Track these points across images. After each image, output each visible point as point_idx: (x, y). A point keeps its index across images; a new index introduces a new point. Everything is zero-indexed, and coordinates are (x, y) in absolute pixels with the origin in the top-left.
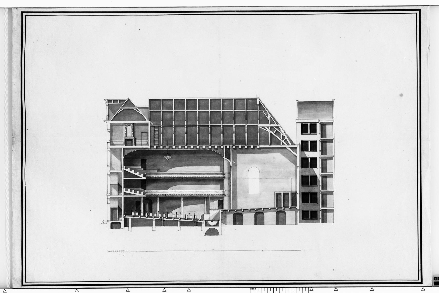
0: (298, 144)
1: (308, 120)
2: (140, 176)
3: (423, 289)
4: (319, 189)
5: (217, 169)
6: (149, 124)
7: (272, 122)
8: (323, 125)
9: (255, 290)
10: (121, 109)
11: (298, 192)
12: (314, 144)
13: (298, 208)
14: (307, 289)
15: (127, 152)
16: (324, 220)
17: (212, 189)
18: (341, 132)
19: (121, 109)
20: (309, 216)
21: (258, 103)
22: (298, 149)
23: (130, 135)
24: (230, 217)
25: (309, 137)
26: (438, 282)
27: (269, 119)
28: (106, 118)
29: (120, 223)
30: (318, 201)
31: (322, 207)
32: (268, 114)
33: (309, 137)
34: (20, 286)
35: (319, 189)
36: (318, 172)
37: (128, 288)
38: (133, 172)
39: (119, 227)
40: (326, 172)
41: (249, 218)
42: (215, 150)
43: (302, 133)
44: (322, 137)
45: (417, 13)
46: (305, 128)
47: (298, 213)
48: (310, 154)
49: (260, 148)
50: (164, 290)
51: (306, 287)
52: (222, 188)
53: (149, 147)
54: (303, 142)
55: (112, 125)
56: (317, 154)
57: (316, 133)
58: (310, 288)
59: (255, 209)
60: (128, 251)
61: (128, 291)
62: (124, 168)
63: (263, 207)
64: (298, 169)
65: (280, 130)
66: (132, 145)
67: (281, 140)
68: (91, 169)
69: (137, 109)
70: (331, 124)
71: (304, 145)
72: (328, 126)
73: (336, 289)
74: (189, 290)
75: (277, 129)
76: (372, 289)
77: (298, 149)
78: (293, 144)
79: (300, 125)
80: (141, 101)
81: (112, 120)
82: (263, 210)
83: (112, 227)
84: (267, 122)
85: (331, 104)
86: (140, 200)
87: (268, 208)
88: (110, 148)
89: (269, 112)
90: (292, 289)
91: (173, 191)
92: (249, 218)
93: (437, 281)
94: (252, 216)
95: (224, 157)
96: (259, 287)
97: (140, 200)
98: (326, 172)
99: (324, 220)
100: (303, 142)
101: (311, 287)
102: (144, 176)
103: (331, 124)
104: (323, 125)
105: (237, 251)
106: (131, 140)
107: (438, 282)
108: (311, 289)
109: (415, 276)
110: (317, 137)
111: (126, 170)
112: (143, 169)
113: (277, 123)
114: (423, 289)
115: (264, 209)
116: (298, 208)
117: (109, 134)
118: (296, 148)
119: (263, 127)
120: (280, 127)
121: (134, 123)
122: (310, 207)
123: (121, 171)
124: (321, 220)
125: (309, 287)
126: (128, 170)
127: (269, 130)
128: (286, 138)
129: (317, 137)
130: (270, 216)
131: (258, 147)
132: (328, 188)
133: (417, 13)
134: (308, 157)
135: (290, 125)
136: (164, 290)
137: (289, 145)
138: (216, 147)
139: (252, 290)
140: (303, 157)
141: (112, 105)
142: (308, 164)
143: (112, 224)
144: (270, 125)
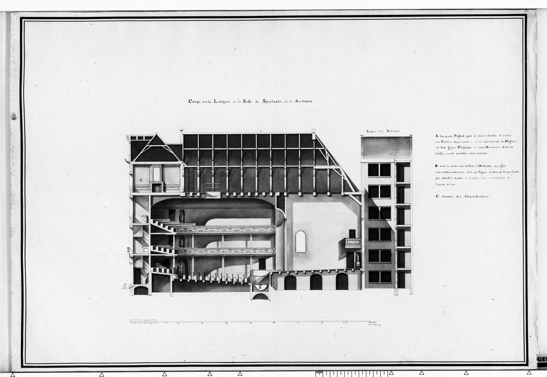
0: (364, 190)
2: (169, 231)
3: (529, 373)
5: (267, 222)
7: (331, 163)
8: (401, 167)
9: (321, 374)
10: (147, 147)
12: (386, 191)
14: (386, 372)
15: (156, 201)
16: (401, 284)
17: (261, 246)
20: (378, 278)
21: (314, 138)
23: (157, 179)
24: (281, 281)
25: (379, 181)
26: (545, 363)
28: (129, 159)
29: (147, 289)
30: (368, 255)
32: (327, 152)
33: (379, 181)
34: (19, 369)
35: (393, 245)
36: (392, 223)
38: (161, 226)
39: (147, 293)
40: (404, 203)
41: (303, 282)
42: (256, 197)
43: (369, 175)
44: (398, 202)
46: (373, 170)
47: (363, 275)
48: (380, 202)
49: (345, 196)
52: (274, 245)
54: (370, 187)
55: (134, 166)
56: (391, 202)
58: (389, 372)
59: (311, 271)
61: (165, 375)
62: (151, 221)
63: (320, 268)
64: (363, 222)
66: (160, 192)
68: (95, 216)
70: (408, 165)
71: (373, 191)
72: (406, 169)
73: (422, 373)
74: (240, 374)
78: (356, 190)
79: (367, 164)
81: (136, 161)
82: (322, 273)
83: (135, 293)
85: (408, 139)
86: (172, 260)
87: (327, 270)
88: (134, 196)
91: (212, 248)
92: (303, 282)
93: (542, 362)
94: (307, 279)
95: (276, 207)
97: (172, 260)
99: (401, 284)
100: (370, 187)
101: (391, 371)
102: (175, 230)
103: (408, 165)
104: (401, 167)
106: (159, 185)
107: (545, 363)
108: (391, 373)
110: (391, 181)
111: (154, 224)
112: (169, 220)
113: (338, 164)
115: (322, 271)
117: (132, 178)
118: (360, 196)
120: (341, 170)
121: (163, 165)
122: (379, 267)
123: (147, 224)
124: (396, 285)
126: (156, 224)
130: (329, 281)
132: (406, 245)
134: (377, 205)
135: (354, 168)
136: (210, 374)
138: (264, 194)
139: (317, 374)
140: (371, 205)
142: (375, 213)
143: (136, 289)
144: (328, 167)
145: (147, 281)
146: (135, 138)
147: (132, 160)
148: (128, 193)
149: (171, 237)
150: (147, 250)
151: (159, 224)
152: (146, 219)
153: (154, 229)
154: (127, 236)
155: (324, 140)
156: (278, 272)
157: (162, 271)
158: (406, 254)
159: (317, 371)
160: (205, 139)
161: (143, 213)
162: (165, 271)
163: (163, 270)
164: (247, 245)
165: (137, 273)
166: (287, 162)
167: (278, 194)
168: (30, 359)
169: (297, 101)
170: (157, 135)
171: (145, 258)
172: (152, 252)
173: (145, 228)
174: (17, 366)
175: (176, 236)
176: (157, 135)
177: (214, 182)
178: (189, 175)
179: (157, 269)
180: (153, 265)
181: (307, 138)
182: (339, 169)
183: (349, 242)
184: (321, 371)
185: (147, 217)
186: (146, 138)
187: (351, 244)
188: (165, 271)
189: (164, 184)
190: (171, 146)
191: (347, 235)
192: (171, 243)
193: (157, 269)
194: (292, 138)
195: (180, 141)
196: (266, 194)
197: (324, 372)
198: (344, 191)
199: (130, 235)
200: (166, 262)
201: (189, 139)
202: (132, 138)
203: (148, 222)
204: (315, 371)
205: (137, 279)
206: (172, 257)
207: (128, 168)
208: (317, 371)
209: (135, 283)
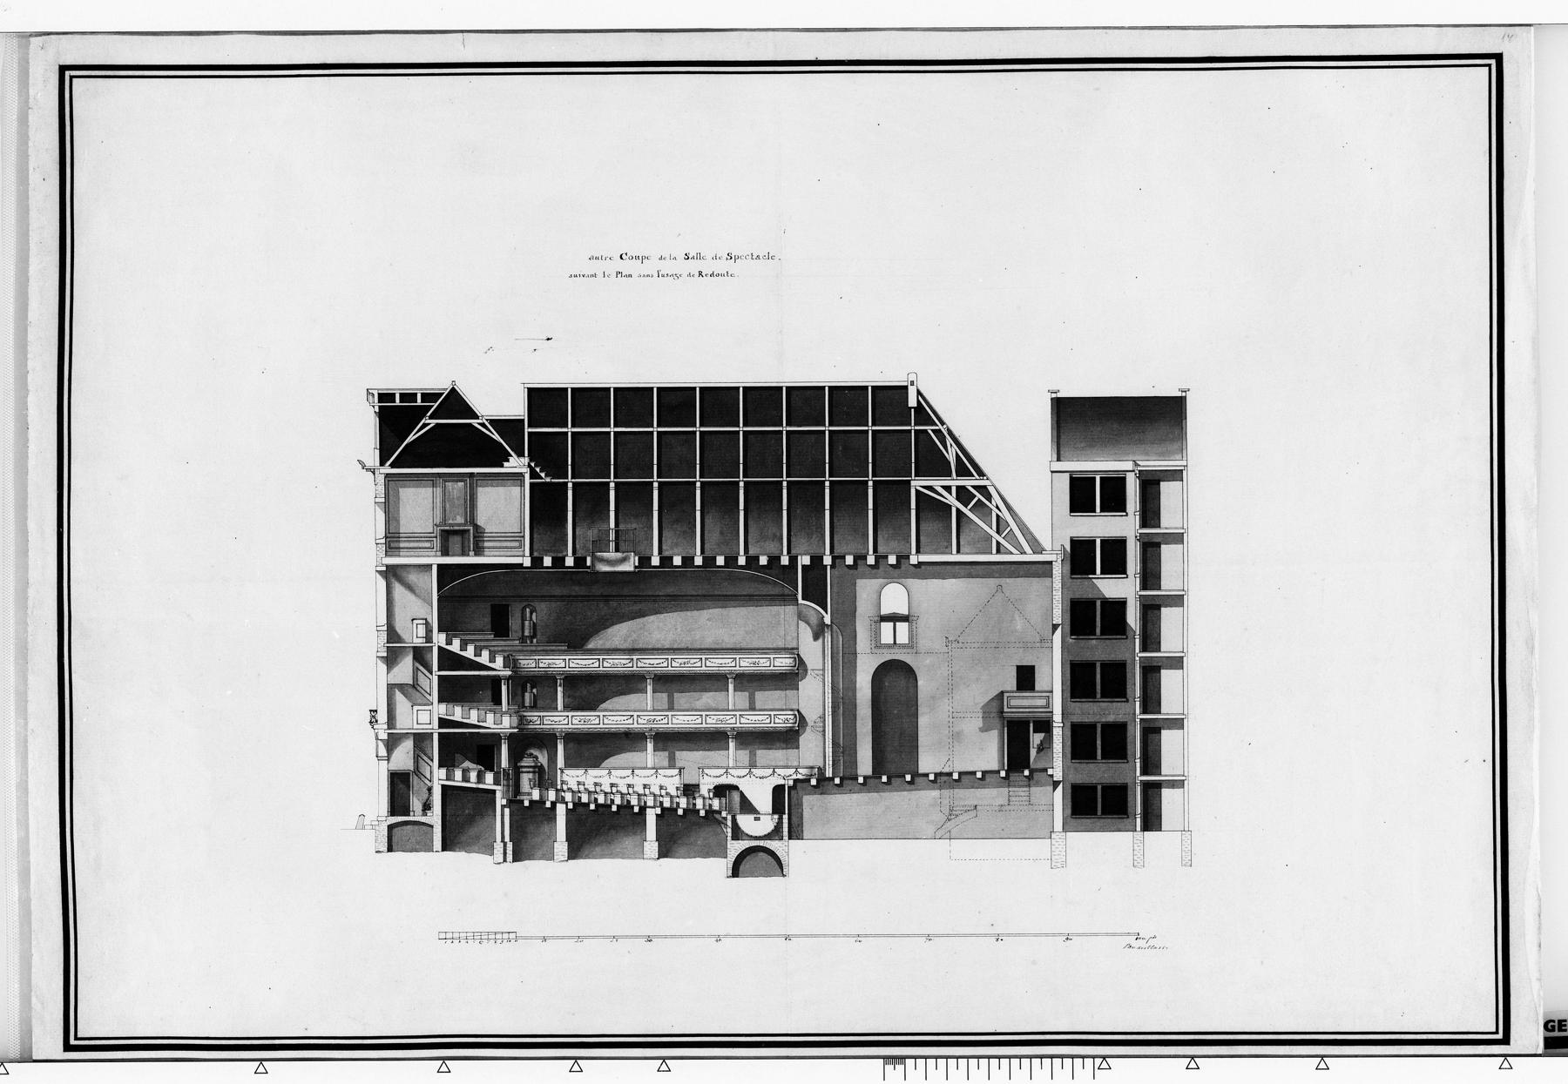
1: (1098, 464)
3: (1506, 1065)
4: (1132, 712)
6: (527, 476)
7: (963, 471)
9: (900, 1068)
10: (425, 425)
11: (1057, 718)
12: (1114, 554)
13: (1058, 776)
14: (1089, 1061)
16: (1152, 821)
18: (1215, 503)
19: (425, 425)
20: (1096, 805)
21: (912, 402)
22: (1057, 570)
25: (1099, 526)
26: (1565, 1038)
27: (952, 458)
28: (373, 458)
31: (1144, 711)
32: (949, 441)
33: (1099, 526)
34: (57, 1051)
35: (1132, 712)
37: (444, 1059)
38: (469, 653)
40: (1159, 588)
44: (1145, 585)
46: (1082, 495)
49: (920, 564)
51: (936, 1057)
53: (527, 562)
57: (1124, 509)
58: (1098, 1061)
60: (511, 936)
62: (440, 639)
65: (989, 497)
66: (464, 553)
67: (993, 533)
68: (278, 617)
69: (483, 425)
70: (1176, 475)
71: (1081, 555)
73: (1193, 1065)
74: (664, 1067)
75: (979, 496)
77: (1057, 570)
78: (1037, 548)
80: (497, 398)
81: (392, 466)
84: (942, 469)
89: (950, 432)
90: (1015, 1062)
91: (612, 717)
93: (1556, 1034)
96: (989, 1057)
98: (1159, 588)
99: (1152, 821)
101: (1104, 1057)
103: (1176, 475)
104: (1151, 484)
106: (463, 533)
108: (1104, 1065)
110: (1125, 526)
113: (981, 474)
114: (1506, 1065)
116: (1058, 776)
119: (930, 488)
120: (991, 489)
122: (1099, 772)
125: (1094, 1057)
126: (455, 647)
127: (951, 499)
129: (1125, 526)
131: (914, 560)
132: (1164, 522)
135: (1028, 481)
139: (889, 1068)
144: (955, 482)
145: (427, 807)
146: (391, 397)
147: (382, 463)
148: (371, 557)
149: (496, 682)
150: (426, 716)
151: (463, 648)
152: (422, 631)
153: (448, 659)
154: (369, 681)
155: (940, 403)
156: (950, 774)
157: (467, 776)
158: (1163, 732)
159: (886, 1058)
160: (590, 401)
161: (419, 613)
162: (480, 778)
163: (473, 776)
164: (522, 719)
165: (399, 785)
166: (832, 467)
167: (805, 560)
168: (91, 1025)
169: (700, 274)
170: (453, 390)
171: (421, 740)
172: (443, 723)
173: (420, 655)
174: (49, 1040)
175: (508, 679)
176: (453, 390)
177: (617, 524)
178: (546, 509)
179: (458, 774)
180: (447, 762)
181: (891, 399)
182: (985, 487)
183: (1014, 702)
184: (901, 1059)
185: (428, 625)
186: (425, 397)
187: (1023, 704)
188: (480, 778)
189: (476, 527)
190: (498, 424)
191: (1011, 683)
192: (497, 700)
193: (458, 774)
194: (847, 399)
195: (516, 408)
196: (899, 558)
197: (910, 1062)
198: (918, 551)
199: (380, 676)
200: (481, 749)
201: (543, 401)
202: (385, 397)
203: (429, 638)
204: (884, 1057)
205: (398, 804)
206: (496, 738)
207: (369, 488)
208: (888, 1059)
209: (393, 811)
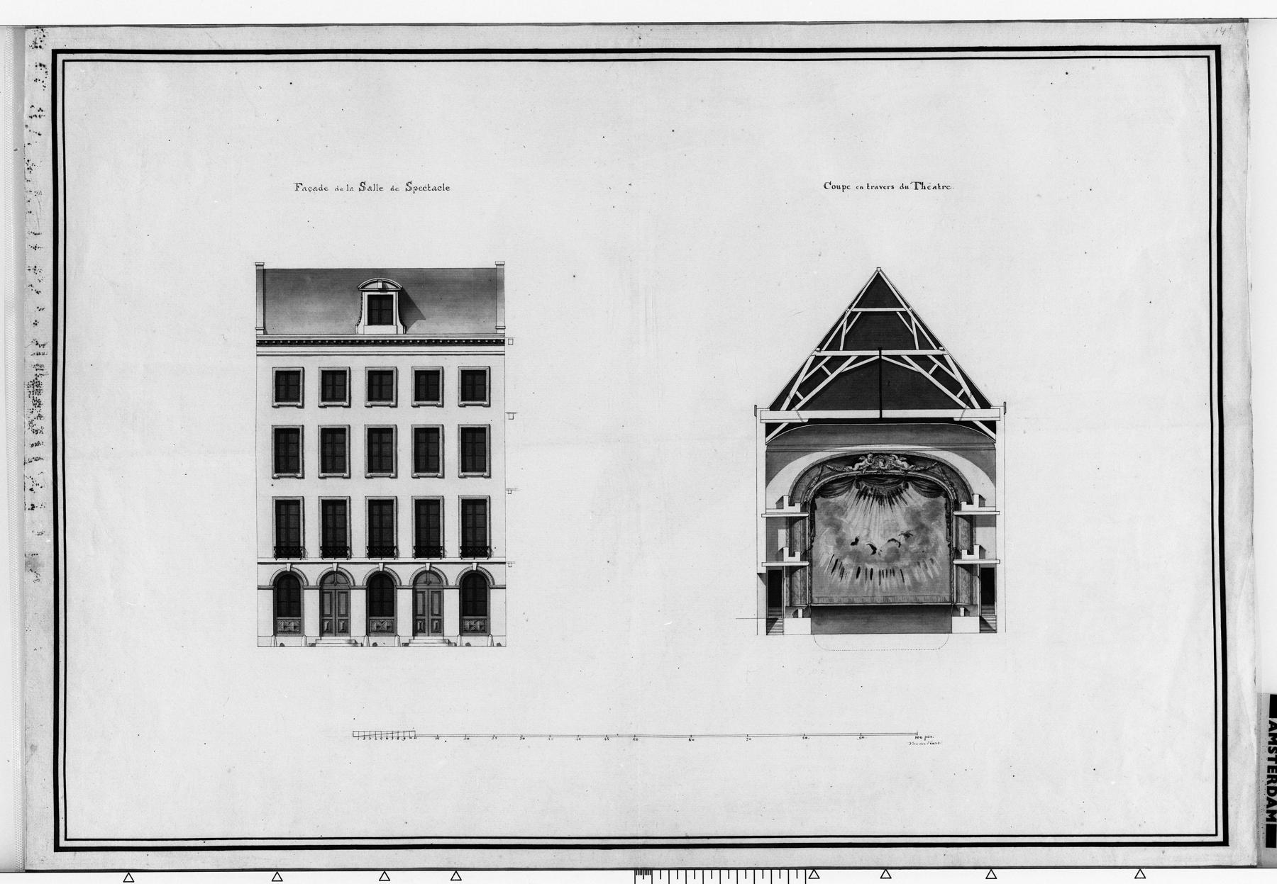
7: (924, 345)
9: (648, 877)
32: (914, 320)
45: (1208, 57)
50: (385, 877)
58: (809, 872)
61: (277, 878)
73: (886, 875)
75: (938, 363)
76: (991, 875)
85: (486, 286)
105: (839, 735)
108: (814, 875)
109: (1205, 823)
113: (938, 345)
120: (947, 358)
128: (966, 388)
133: (1208, 57)
137: (973, 407)
139: (639, 877)
141: (879, 314)
